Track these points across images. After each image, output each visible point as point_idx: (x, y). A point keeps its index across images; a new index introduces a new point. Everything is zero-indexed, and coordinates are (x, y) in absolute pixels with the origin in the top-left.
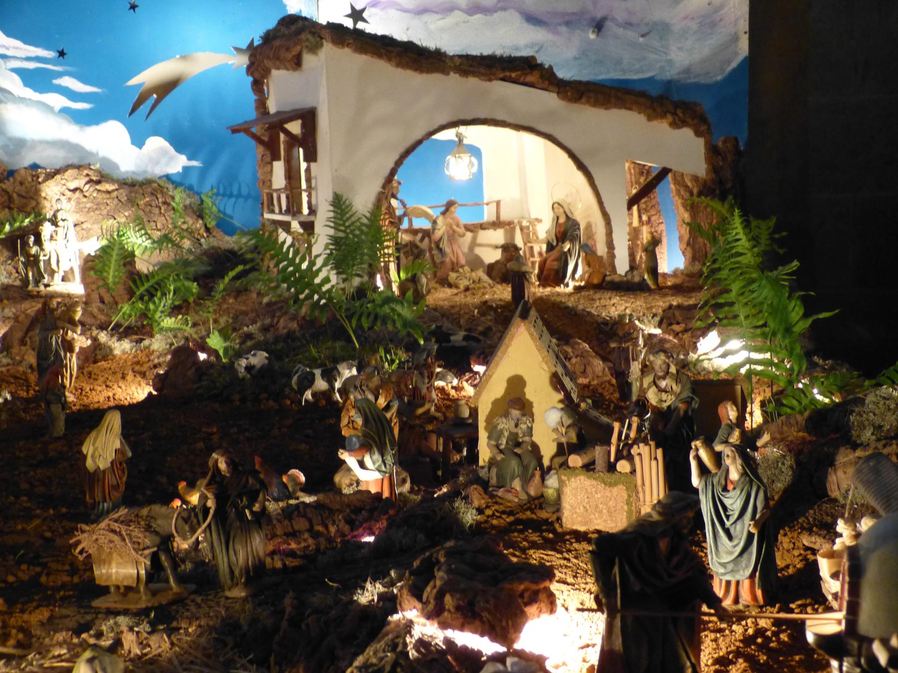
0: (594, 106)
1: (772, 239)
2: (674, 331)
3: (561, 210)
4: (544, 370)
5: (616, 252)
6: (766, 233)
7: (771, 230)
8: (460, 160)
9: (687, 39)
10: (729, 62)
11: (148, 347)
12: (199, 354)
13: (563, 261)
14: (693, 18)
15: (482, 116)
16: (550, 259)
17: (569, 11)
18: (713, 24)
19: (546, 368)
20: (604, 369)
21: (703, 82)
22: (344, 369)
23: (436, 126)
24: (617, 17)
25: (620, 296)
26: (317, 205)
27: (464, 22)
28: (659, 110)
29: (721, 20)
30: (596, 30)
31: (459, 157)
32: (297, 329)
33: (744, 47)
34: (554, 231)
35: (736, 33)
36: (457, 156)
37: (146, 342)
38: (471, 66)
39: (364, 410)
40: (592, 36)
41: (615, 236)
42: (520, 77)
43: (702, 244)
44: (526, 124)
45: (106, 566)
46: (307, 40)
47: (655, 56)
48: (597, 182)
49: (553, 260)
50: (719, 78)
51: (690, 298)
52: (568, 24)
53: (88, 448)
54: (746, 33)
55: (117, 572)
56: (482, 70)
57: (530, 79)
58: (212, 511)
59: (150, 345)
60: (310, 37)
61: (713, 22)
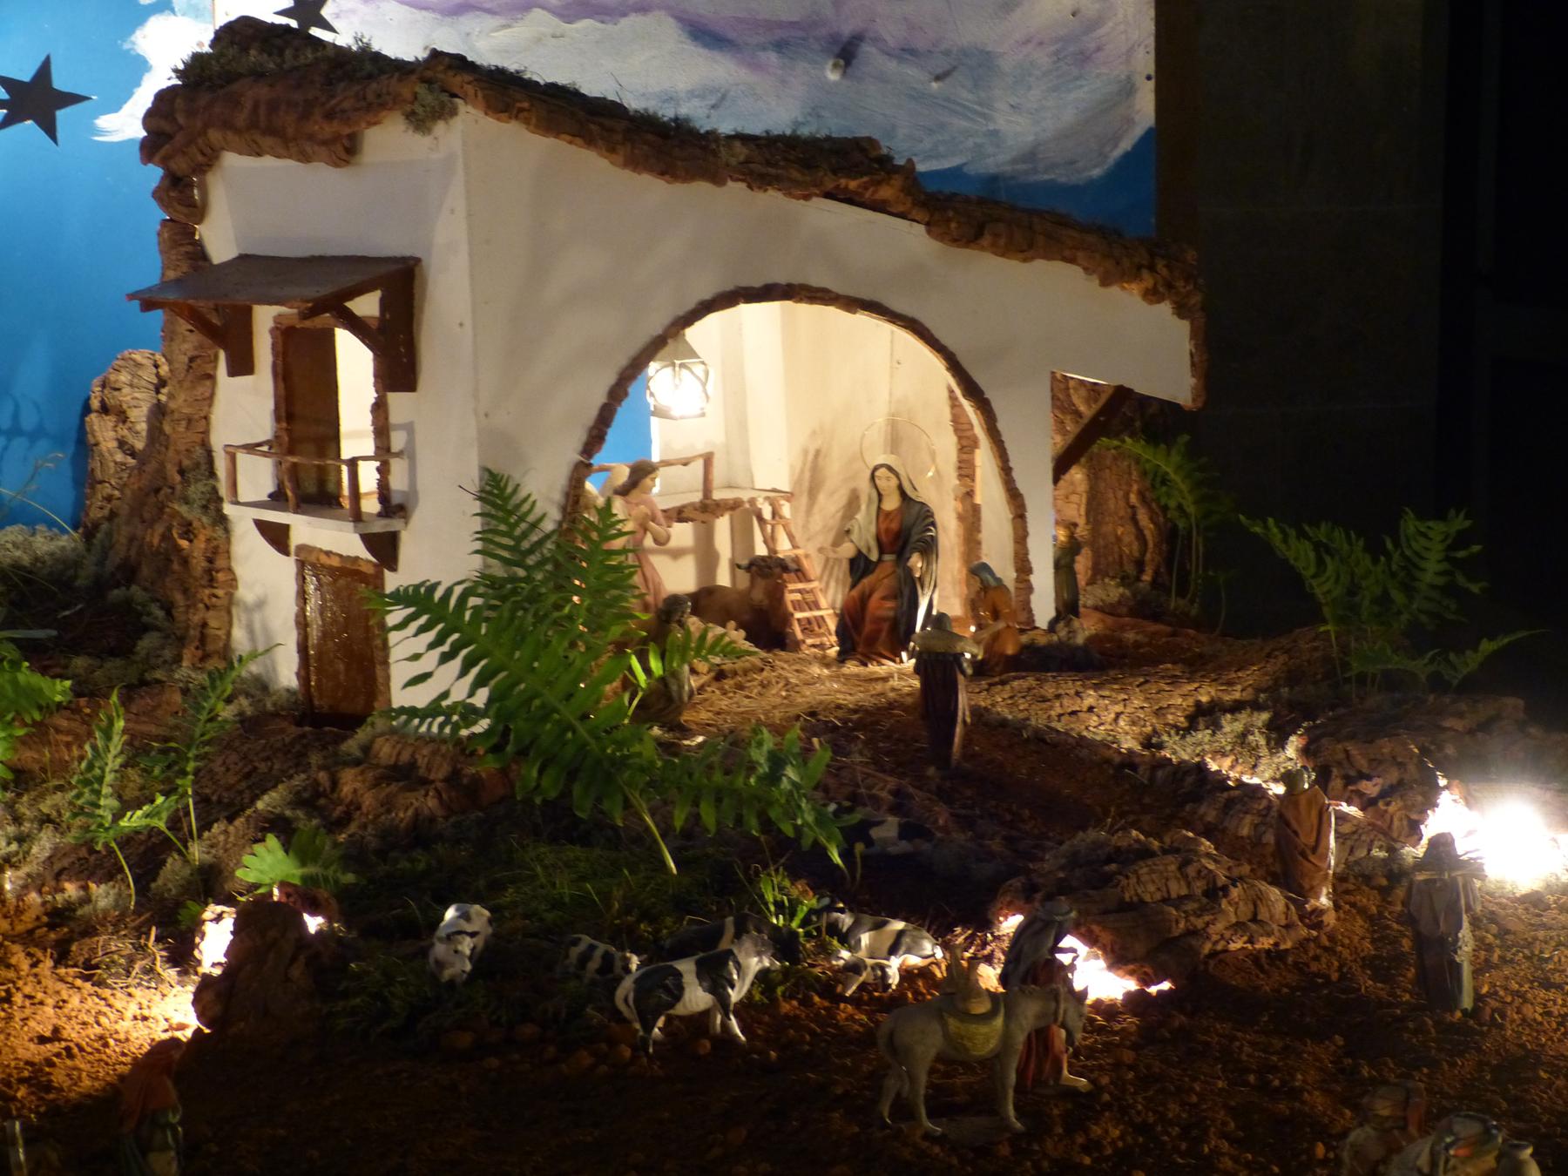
0: (1003, 255)
1: (1447, 559)
2: (1360, 794)
3: (894, 482)
5: (1033, 579)
6: (1441, 547)
7: (1449, 541)
8: (684, 372)
9: (1030, 88)
10: (1116, 140)
12: (306, 917)
13: (905, 600)
14: (1041, 43)
15: (781, 278)
16: (876, 596)
17: (784, 18)
18: (1083, 58)
20: (1288, 908)
21: (1063, 180)
22: (748, 955)
23: (690, 304)
24: (888, 38)
25: (1096, 687)
26: (412, 493)
27: (554, 36)
28: (1126, 262)
29: (1099, 49)
30: (842, 62)
31: (682, 366)
32: (440, 812)
33: (1145, 107)
34: (873, 529)
35: (1129, 78)
36: (678, 362)
38: (768, 163)
40: (833, 76)
41: (1032, 543)
42: (866, 189)
43: (1112, 539)
44: (866, 294)
46: (415, 96)
47: (964, 124)
48: (1001, 425)
49: (884, 598)
50: (1096, 172)
51: (1230, 683)
52: (780, 46)
54: (1149, 78)
56: (795, 174)
57: (885, 193)
60: (421, 89)
61: (1082, 53)
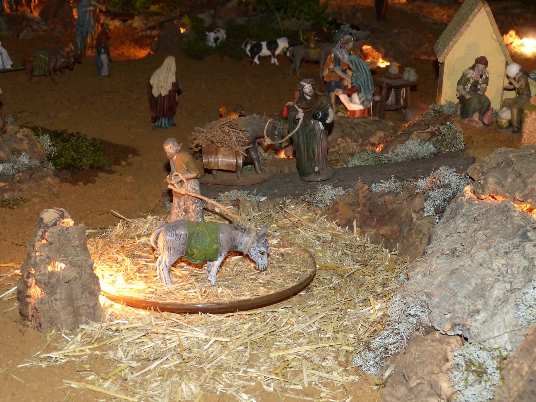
4: (494, 39)
11: (130, 25)
19: (495, 37)
37: (130, 22)
39: (355, 63)
45: (213, 156)
53: (153, 81)
55: (222, 160)
58: (300, 121)
59: (132, 23)
